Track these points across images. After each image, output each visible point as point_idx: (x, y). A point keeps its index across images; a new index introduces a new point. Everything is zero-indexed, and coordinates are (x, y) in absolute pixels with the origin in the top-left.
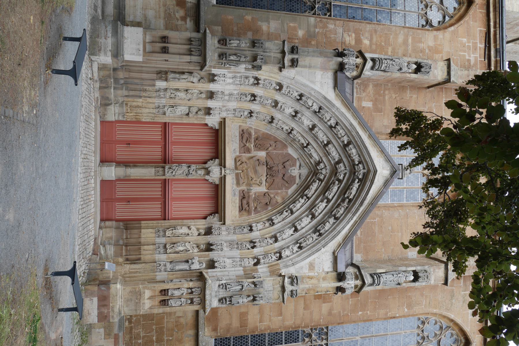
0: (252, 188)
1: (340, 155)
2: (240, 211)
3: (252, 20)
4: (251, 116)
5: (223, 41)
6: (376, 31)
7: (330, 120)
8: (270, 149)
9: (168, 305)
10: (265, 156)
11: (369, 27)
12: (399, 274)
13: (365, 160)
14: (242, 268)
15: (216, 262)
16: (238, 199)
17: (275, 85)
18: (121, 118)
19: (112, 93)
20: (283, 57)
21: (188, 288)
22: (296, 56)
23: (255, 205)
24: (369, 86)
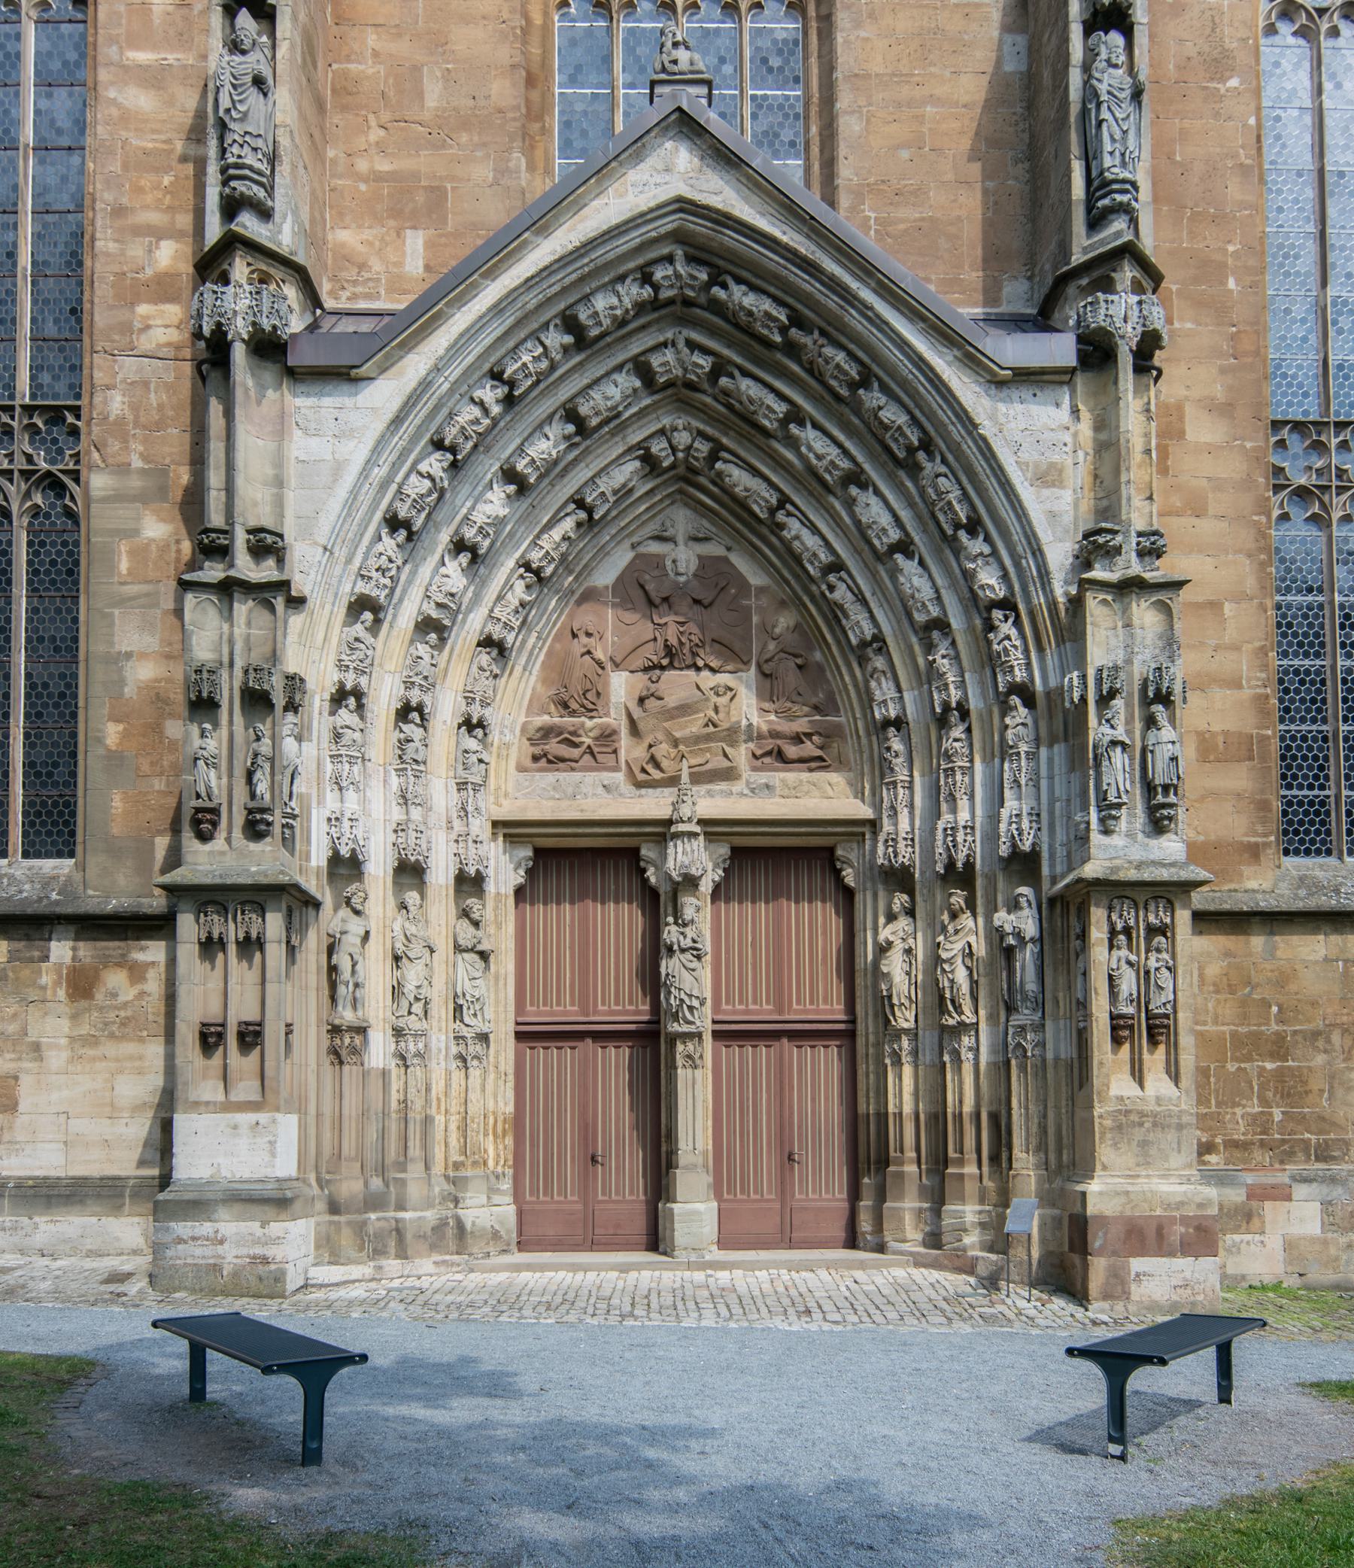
0: (744, 722)
1: (619, 368)
3: (118, 721)
5: (198, 822)
8: (599, 654)
9: (1167, 1016)
11: (105, 241)
14: (1043, 752)
15: (1014, 846)
16: (782, 775)
17: (359, 627)
18: (506, 1185)
19: (418, 1216)
20: (249, 588)
21: (1111, 947)
22: (241, 538)
24: (343, 245)
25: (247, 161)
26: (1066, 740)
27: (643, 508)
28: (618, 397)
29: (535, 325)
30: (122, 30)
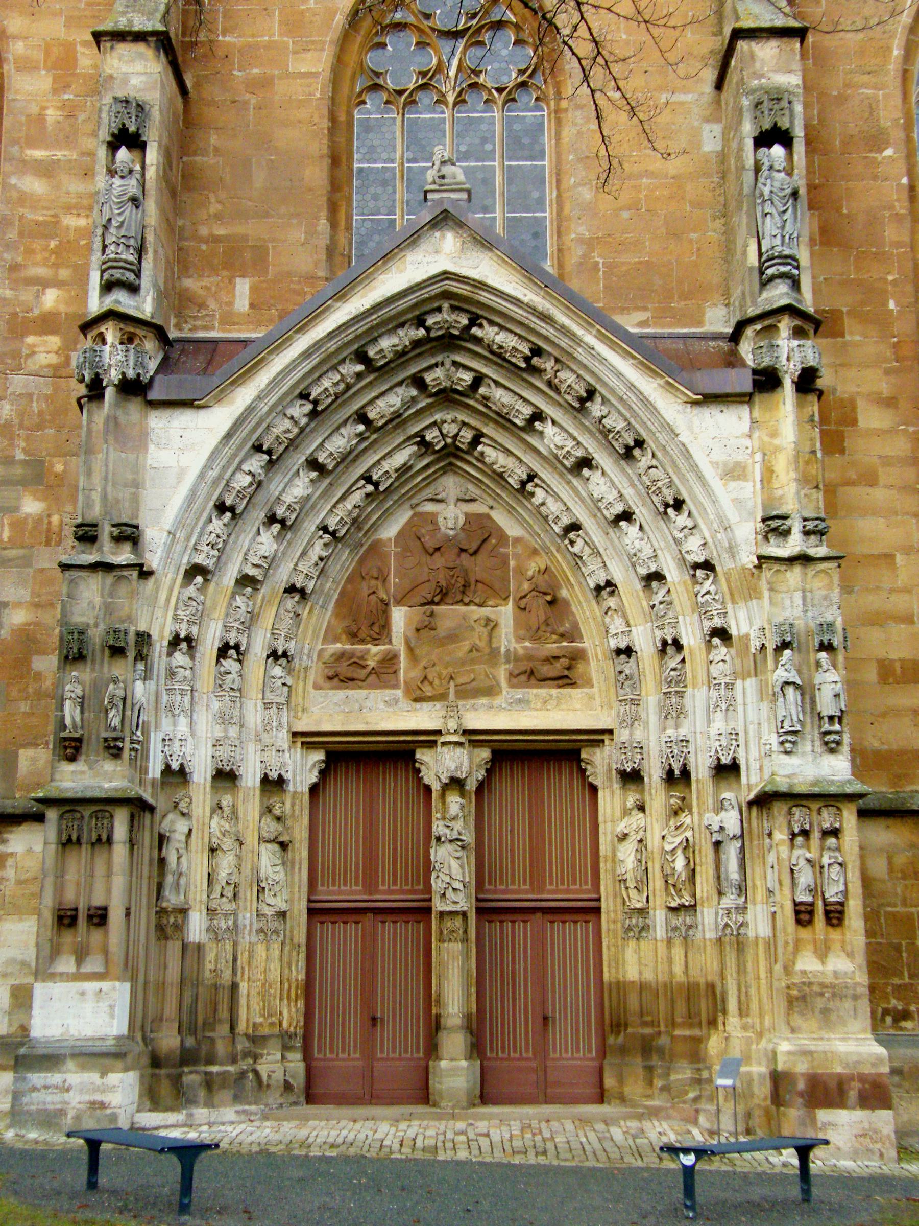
0: (503, 650)
1: (400, 384)
2: (573, 685)
4: (285, 655)
7: (292, 418)
9: (842, 904)
10: (405, 609)
12: (762, 195)
13: (416, 307)
15: (719, 759)
16: (535, 691)
21: (792, 846)
23: (555, 637)
25: (123, 257)
26: (756, 676)
27: (420, 478)
28: (399, 404)
29: (336, 361)
30: (22, 134)
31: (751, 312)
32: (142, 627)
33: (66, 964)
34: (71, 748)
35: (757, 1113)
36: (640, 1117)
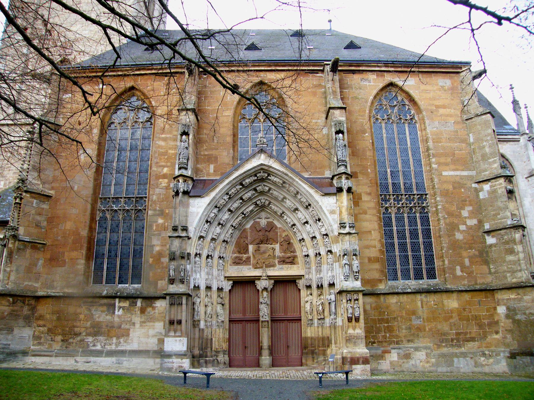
2: (294, 264)
4: (223, 257)
6: (157, 163)
11: (154, 169)
31: (336, 173)
32: (188, 251)
33: (172, 333)
34: (172, 281)
35: (339, 367)
36: (311, 369)
